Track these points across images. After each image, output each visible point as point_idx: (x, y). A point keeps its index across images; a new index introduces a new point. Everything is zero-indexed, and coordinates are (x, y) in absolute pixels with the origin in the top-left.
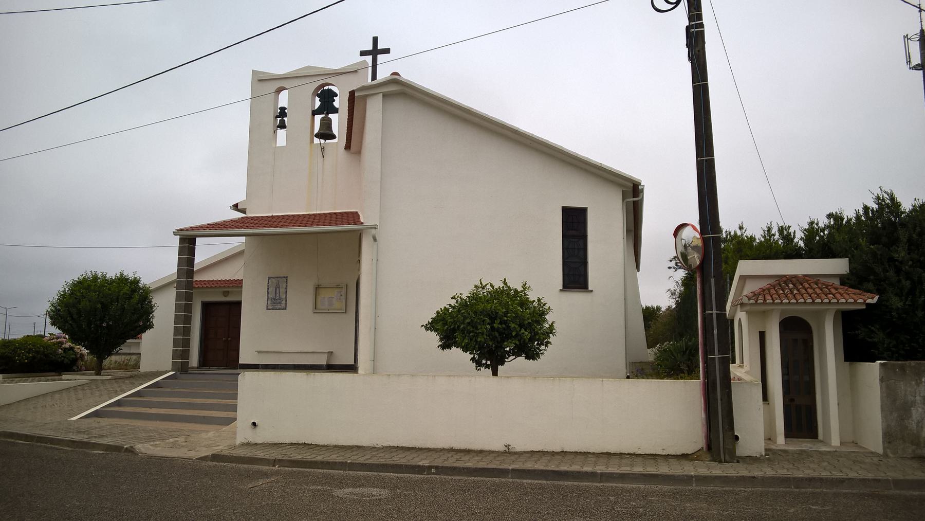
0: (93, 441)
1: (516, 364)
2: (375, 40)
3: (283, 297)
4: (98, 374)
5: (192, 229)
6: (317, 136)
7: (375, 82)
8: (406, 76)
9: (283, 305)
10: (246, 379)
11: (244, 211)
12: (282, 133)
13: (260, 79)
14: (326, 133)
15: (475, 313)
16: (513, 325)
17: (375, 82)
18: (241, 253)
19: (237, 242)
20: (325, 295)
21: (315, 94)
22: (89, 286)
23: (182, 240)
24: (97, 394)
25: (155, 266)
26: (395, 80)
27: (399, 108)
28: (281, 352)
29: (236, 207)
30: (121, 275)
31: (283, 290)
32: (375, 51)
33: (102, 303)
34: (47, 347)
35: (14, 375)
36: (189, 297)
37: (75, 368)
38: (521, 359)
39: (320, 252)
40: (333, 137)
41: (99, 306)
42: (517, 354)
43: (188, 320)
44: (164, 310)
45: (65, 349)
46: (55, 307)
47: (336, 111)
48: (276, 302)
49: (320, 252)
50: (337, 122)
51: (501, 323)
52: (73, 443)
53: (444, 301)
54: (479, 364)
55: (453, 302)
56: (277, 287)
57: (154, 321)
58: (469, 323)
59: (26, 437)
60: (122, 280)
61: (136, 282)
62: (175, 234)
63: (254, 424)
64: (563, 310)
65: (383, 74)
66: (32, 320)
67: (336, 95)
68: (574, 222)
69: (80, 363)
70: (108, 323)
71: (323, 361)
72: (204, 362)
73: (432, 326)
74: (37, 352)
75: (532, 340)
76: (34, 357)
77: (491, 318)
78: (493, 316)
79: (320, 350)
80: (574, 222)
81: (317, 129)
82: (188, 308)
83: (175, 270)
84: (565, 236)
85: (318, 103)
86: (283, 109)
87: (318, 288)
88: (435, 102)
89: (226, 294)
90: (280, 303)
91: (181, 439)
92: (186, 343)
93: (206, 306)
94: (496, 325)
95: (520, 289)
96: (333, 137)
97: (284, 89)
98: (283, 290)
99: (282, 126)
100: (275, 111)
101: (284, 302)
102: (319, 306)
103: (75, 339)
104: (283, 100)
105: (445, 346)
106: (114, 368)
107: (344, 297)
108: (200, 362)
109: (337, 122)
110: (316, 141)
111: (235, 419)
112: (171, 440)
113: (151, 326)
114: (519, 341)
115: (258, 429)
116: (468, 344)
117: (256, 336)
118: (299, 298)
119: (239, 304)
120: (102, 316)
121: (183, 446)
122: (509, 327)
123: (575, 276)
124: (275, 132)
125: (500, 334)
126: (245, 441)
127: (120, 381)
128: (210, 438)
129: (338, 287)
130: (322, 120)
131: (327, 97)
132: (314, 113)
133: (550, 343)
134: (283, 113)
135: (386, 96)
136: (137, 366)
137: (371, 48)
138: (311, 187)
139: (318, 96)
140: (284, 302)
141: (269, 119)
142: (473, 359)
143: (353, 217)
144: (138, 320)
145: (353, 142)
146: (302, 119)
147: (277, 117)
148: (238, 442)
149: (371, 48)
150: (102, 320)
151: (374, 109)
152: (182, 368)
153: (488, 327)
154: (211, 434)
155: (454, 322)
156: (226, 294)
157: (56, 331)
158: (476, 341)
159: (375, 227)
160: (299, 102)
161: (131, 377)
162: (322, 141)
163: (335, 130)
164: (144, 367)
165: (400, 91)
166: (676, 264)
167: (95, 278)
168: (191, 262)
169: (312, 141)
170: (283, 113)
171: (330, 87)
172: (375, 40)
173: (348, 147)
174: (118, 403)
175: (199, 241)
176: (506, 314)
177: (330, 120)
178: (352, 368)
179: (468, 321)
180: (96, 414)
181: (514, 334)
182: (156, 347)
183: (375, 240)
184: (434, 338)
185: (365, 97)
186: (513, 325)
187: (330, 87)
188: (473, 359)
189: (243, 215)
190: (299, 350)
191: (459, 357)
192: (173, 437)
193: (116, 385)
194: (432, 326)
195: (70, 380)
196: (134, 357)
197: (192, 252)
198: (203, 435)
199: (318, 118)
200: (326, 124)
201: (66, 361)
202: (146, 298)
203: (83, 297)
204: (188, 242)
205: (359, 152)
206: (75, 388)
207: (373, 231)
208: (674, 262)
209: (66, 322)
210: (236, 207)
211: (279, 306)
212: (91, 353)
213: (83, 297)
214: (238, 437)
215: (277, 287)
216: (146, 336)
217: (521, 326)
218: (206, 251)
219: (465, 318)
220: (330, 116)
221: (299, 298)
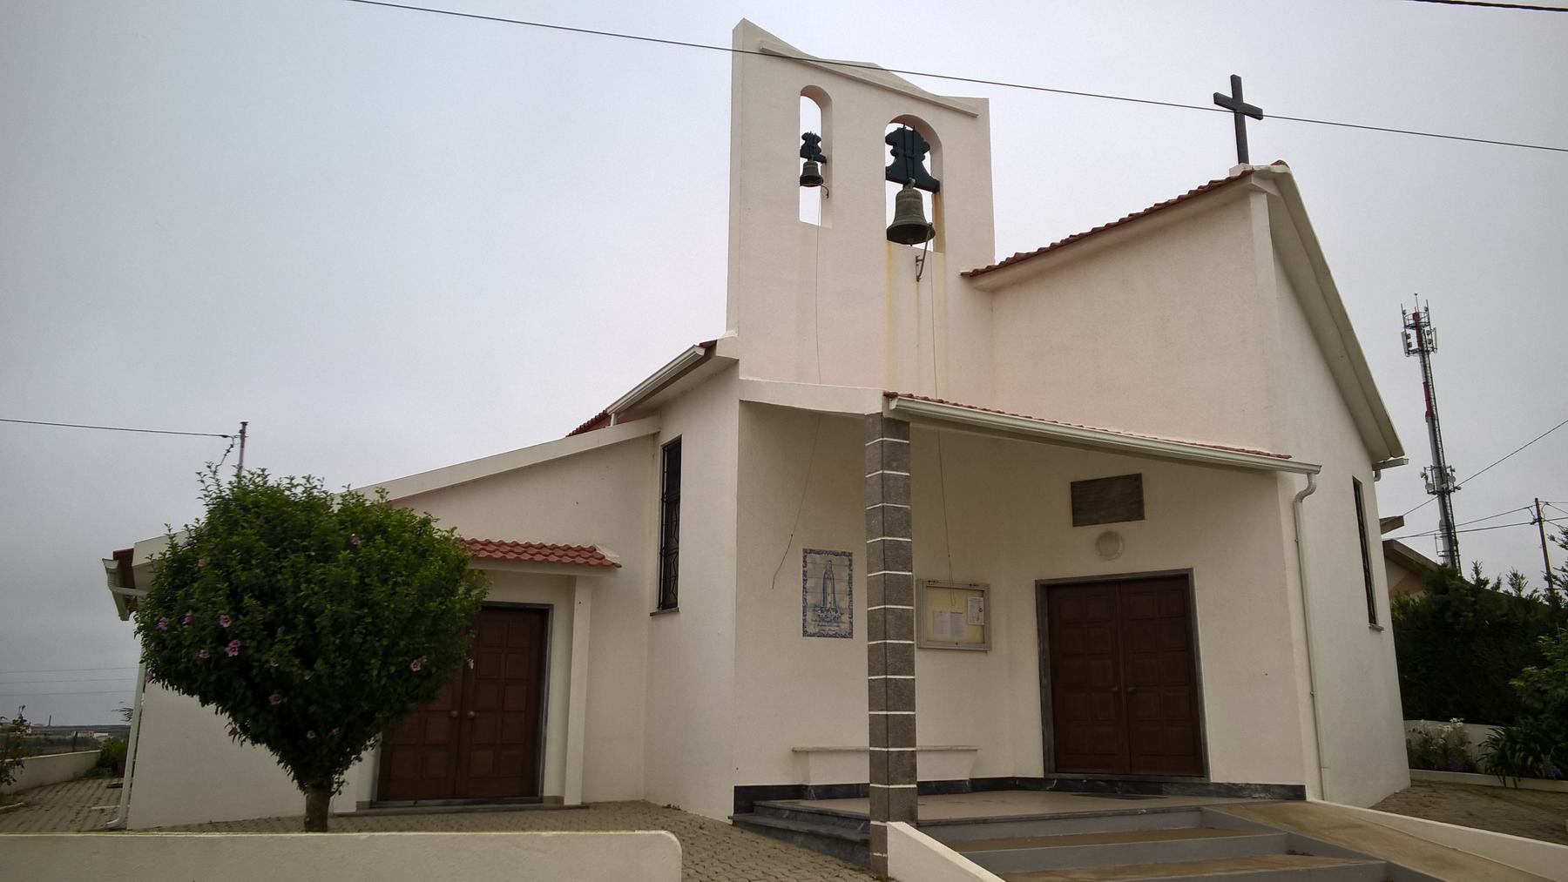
3: (844, 604)
31: (841, 587)
56: (828, 578)
57: (258, 746)
90: (837, 620)
98: (841, 587)
101: (845, 618)
140: (845, 618)
211: (834, 628)
215: (828, 578)
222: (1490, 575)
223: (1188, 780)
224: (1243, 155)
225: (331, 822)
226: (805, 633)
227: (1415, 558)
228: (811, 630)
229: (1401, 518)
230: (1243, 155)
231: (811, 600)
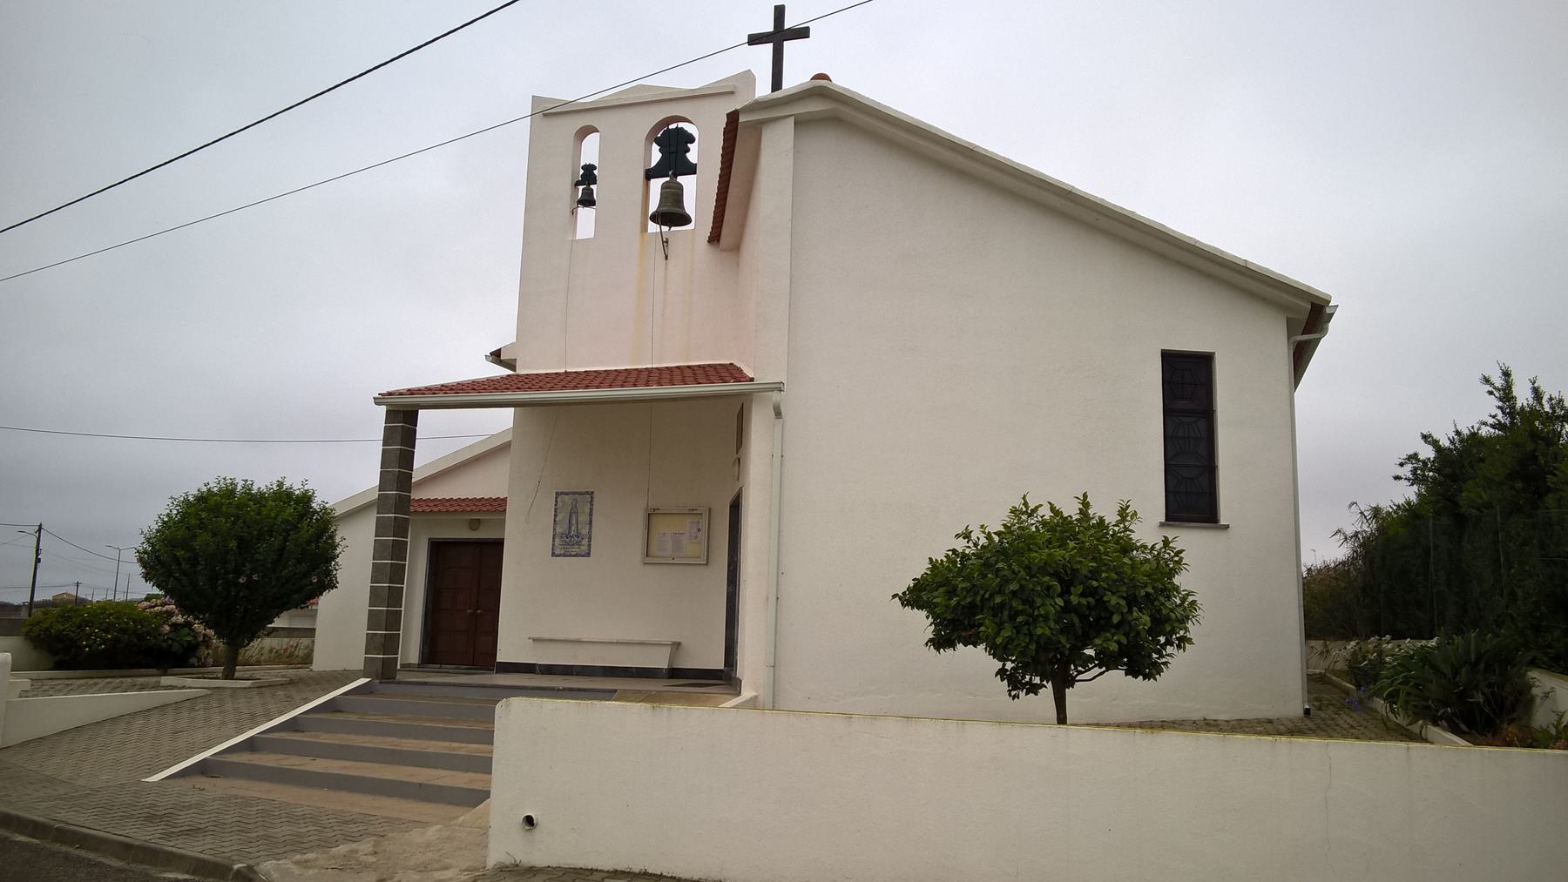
0: (168, 846)
1: (1102, 688)
2: (779, 12)
3: (585, 531)
4: (229, 675)
5: (411, 392)
6: (654, 218)
7: (778, 94)
8: (841, 80)
9: (584, 548)
10: (519, 720)
11: (510, 365)
12: (585, 214)
13: (548, 112)
14: (671, 215)
15: (1028, 568)
16: (1114, 600)
17: (778, 94)
18: (504, 448)
19: (501, 420)
20: (663, 527)
21: (653, 137)
22: (218, 505)
23: (391, 415)
24: (217, 719)
25: (344, 475)
26: (820, 89)
27: (829, 149)
28: (579, 642)
29: (496, 356)
30: (280, 484)
31: (583, 518)
32: (780, 35)
33: (241, 540)
34: (140, 620)
35: (79, 673)
36: (401, 528)
37: (193, 660)
38: (1117, 676)
39: (662, 445)
40: (685, 220)
41: (233, 544)
42: (1108, 661)
43: (397, 574)
44: (356, 554)
45: (175, 626)
46: (152, 545)
47: (691, 169)
48: (571, 541)
49: (662, 445)
50: (695, 192)
51: (1083, 595)
52: (126, 850)
53: (941, 544)
54: (1015, 683)
55: (960, 544)
56: (574, 512)
57: (340, 576)
58: (1014, 593)
59: (36, 829)
60: (283, 496)
61: (306, 498)
62: (378, 401)
63: (529, 821)
64: (1201, 563)
65: (793, 79)
66: (110, 573)
67: (692, 140)
68: (1188, 383)
69: (203, 651)
70: (249, 577)
71: (661, 661)
72: (432, 654)
73: (915, 597)
74: (124, 631)
75: (1154, 631)
76: (116, 640)
77: (1061, 581)
78: (1067, 578)
79: (656, 639)
80: (1188, 383)
81: (654, 206)
82: (398, 550)
83: (375, 481)
84: (1168, 412)
85: (656, 155)
86: (589, 169)
87: (650, 516)
88: (903, 136)
89: (475, 524)
90: (579, 543)
91: (365, 846)
92: (393, 620)
93: (439, 550)
94: (1074, 599)
95: (1111, 518)
96: (685, 220)
97: (594, 130)
98: (583, 518)
99: (588, 201)
100: (574, 172)
101: (585, 542)
102: (654, 549)
103: (184, 608)
104: (590, 151)
105: (941, 642)
106: (267, 662)
107: (703, 536)
108: (422, 653)
109: (695, 192)
110: (653, 227)
111: (486, 795)
112: (343, 849)
113: (332, 585)
114: (1126, 635)
115: (537, 831)
116: (1010, 639)
117: (533, 610)
118: (617, 532)
119: (499, 544)
120: (237, 564)
121: (367, 866)
122: (1101, 603)
123: (1192, 493)
124: (573, 212)
125: (1083, 617)
126: (508, 861)
127: (267, 691)
128: (428, 845)
129: (692, 512)
130: (664, 187)
131: (674, 144)
132: (650, 174)
133: (1189, 641)
134: (589, 175)
135: (801, 123)
136: (307, 660)
137: (769, 28)
138: (647, 314)
139: (658, 141)
140: (585, 542)
141: (563, 187)
142: (1002, 673)
143: (731, 372)
144: (307, 574)
145: (725, 229)
146: (628, 187)
147: (578, 184)
148: (491, 863)
149: (769, 28)
150: (238, 572)
151: (777, 150)
152: (384, 672)
153: (1060, 602)
154: (432, 832)
155: (973, 589)
156: (475, 524)
157: (152, 589)
158: (1031, 635)
159: (779, 387)
160: (621, 155)
161: (292, 682)
162: (665, 228)
163: (690, 206)
164: (320, 663)
165: (831, 112)
166: (1414, 471)
167: (229, 492)
168: (407, 458)
169: (644, 228)
170: (589, 175)
171: (681, 125)
172: (779, 12)
173: (715, 238)
174: (250, 745)
175: (421, 412)
176: (1094, 574)
177: (680, 187)
178: (724, 678)
179: (1013, 587)
180: (203, 769)
181: (1116, 619)
182: (340, 621)
183: (778, 413)
184: (920, 623)
185: (758, 126)
186: (1114, 600)
187: (681, 125)
188: (1002, 673)
189: (506, 372)
190: (614, 638)
191: (975, 662)
192: (349, 838)
193: (256, 700)
194: (915, 597)
195: (179, 686)
196: (305, 641)
197: (409, 438)
198: (416, 836)
199: (657, 184)
200: (673, 195)
201: (176, 647)
202: (326, 529)
203: (202, 525)
204: (402, 417)
205: (736, 248)
206: (163, 708)
207: (775, 396)
208: (1409, 467)
209: (171, 575)
210: (496, 356)
211: (575, 550)
212: (220, 635)
213: (202, 525)
214: (492, 845)
215: (574, 512)
216: (326, 601)
217: (1132, 601)
218: (441, 437)
219: (1007, 581)
220: (680, 179)
221: (617, 532)
222: (263, 489)
223: (165, 680)
224: (777, 83)
225: (1318, 644)
226: (553, 554)
227: (176, 670)
228: (558, 552)
229: (1172, 361)
230: (777, 83)
231: (559, 530)
